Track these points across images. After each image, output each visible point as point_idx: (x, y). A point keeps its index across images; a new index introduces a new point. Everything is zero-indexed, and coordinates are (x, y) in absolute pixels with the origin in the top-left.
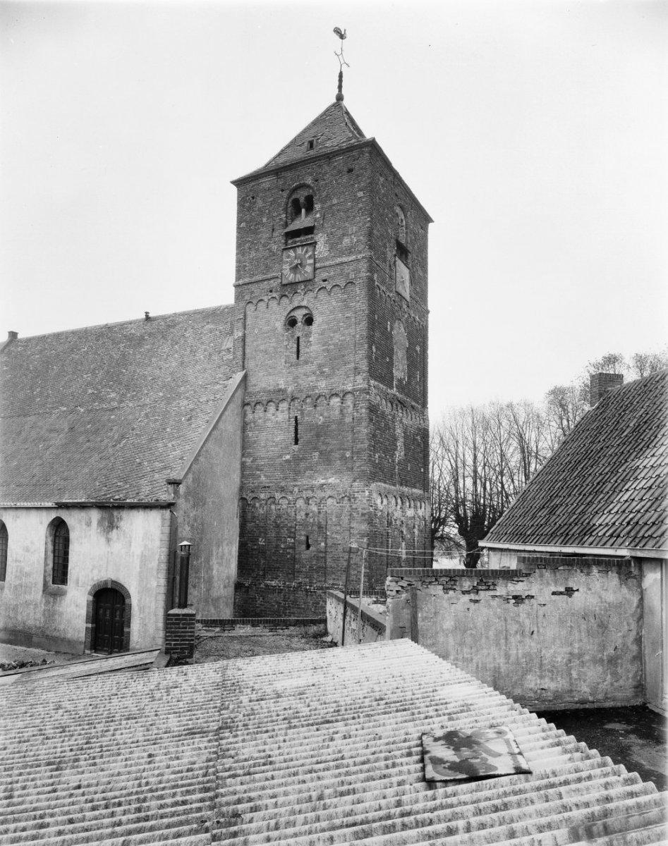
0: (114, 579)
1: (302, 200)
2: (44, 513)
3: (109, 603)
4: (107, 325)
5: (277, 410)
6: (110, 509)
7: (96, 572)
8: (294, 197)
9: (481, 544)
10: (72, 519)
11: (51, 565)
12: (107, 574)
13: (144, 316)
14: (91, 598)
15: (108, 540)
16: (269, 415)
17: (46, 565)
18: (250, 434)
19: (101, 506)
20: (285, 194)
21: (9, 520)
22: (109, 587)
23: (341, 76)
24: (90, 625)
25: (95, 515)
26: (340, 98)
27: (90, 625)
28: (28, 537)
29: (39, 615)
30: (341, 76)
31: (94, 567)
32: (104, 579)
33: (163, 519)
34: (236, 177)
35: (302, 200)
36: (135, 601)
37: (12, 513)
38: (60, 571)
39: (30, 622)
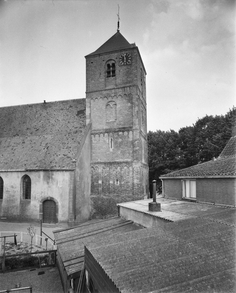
0: (51, 196)
1: (111, 65)
2: (19, 174)
3: (49, 204)
4: (28, 105)
5: (104, 136)
6: (48, 171)
7: (43, 194)
8: (108, 63)
9: (160, 178)
10: (32, 176)
11: (22, 193)
12: (49, 194)
13: (43, 102)
14: (41, 204)
15: (48, 183)
16: (101, 138)
17: (21, 192)
18: (94, 145)
19: (45, 170)
20: (104, 62)
21: (3, 176)
22: (49, 199)
23: (118, 23)
24: (41, 213)
25: (42, 174)
26: (118, 31)
27: (41, 213)
28: (12, 183)
29: (18, 211)
30: (118, 23)
31: (42, 192)
32: (47, 196)
33: (71, 175)
34: (86, 55)
35: (111, 65)
36: (60, 204)
37: (5, 174)
38: (27, 194)
39: (15, 214)
